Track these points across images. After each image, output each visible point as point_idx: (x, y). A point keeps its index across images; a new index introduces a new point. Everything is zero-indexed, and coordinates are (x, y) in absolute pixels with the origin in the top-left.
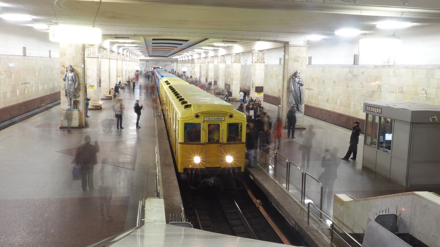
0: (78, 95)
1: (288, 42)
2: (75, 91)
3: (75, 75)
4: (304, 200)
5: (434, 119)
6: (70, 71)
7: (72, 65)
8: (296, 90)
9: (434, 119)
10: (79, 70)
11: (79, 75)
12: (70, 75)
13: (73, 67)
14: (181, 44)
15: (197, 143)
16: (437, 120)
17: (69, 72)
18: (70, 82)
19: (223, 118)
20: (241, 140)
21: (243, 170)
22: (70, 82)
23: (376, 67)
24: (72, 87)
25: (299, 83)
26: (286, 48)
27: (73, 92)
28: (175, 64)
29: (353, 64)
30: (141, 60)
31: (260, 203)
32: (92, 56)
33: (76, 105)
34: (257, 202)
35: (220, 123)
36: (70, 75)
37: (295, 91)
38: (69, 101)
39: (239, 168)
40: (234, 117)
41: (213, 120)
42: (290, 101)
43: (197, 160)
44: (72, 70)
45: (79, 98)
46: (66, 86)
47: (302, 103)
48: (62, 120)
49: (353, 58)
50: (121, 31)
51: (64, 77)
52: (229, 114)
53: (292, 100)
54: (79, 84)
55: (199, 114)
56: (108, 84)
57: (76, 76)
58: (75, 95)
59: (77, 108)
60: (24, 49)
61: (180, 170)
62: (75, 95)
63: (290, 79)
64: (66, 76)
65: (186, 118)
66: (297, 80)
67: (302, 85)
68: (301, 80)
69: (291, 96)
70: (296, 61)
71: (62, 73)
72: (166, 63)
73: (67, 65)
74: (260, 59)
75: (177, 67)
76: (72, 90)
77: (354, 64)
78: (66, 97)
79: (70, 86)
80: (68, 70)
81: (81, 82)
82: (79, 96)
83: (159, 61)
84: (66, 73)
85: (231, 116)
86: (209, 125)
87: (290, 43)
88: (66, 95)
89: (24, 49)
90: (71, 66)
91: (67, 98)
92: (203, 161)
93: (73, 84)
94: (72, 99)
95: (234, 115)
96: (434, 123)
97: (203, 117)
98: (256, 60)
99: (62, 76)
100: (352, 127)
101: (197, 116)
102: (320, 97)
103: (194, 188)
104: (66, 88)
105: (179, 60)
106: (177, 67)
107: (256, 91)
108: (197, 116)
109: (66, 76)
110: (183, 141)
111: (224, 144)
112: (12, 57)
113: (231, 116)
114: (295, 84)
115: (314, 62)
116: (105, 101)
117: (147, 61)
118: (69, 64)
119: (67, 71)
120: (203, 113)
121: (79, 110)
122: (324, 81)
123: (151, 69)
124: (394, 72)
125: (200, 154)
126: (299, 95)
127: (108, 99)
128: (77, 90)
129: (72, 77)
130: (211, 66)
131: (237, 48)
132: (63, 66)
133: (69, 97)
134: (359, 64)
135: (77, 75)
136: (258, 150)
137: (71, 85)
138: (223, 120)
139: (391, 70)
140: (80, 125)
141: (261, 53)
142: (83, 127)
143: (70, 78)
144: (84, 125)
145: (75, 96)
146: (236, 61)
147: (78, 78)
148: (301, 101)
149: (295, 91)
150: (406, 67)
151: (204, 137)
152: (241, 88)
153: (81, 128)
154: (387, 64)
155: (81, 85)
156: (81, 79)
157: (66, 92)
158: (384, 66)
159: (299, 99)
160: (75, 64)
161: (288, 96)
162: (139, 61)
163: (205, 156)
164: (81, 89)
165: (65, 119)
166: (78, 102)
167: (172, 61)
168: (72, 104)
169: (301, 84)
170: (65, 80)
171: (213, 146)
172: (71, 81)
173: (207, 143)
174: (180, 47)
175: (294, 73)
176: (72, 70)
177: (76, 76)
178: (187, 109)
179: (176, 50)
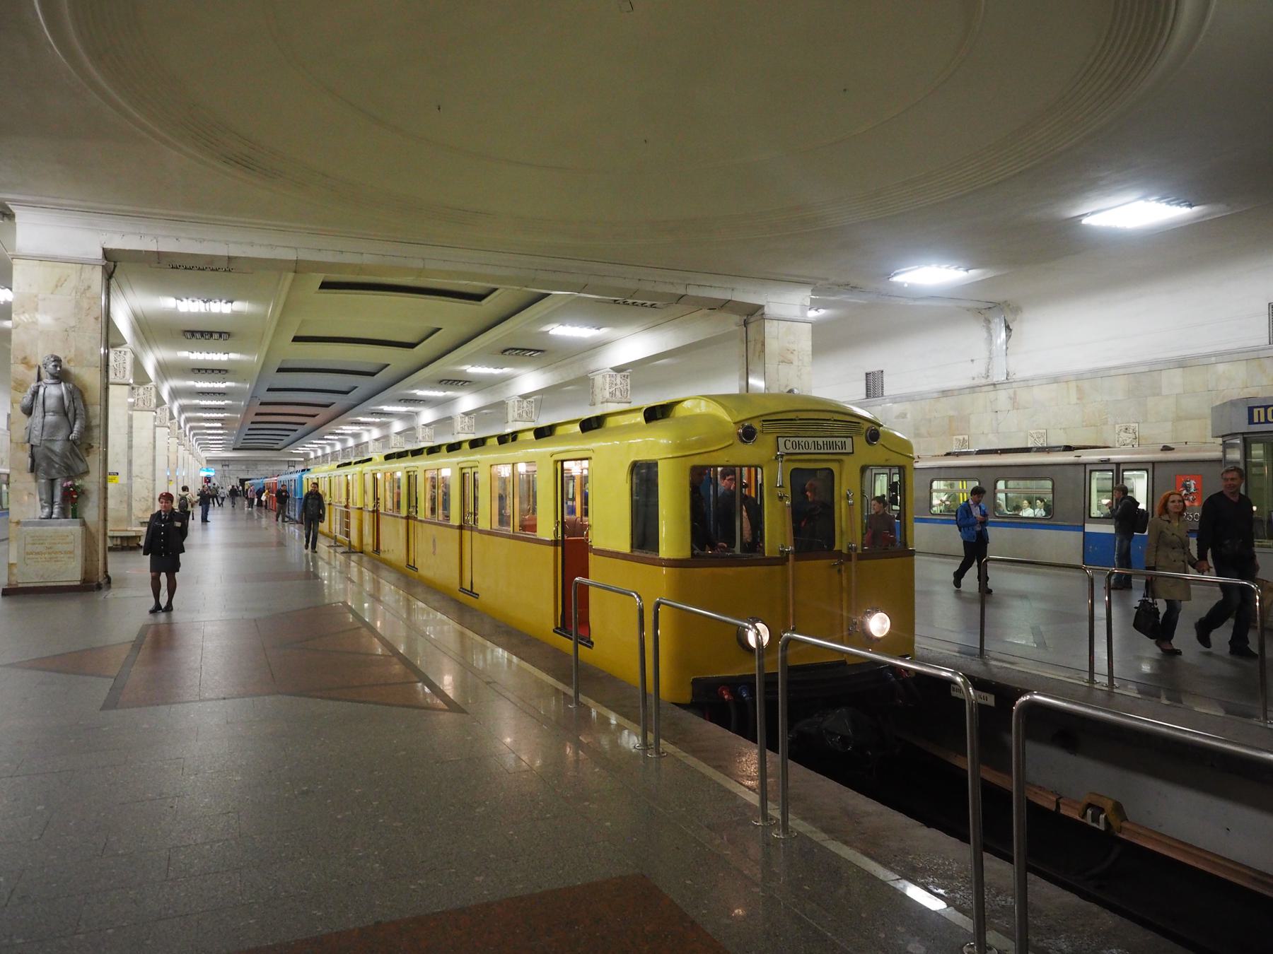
0: (81, 468)
1: (761, 307)
2: (72, 451)
3: (70, 392)
6: (53, 376)
7: (61, 356)
10: (90, 377)
12: (53, 391)
13: (65, 365)
14: (314, 416)
18: (50, 418)
19: (848, 441)
22: (50, 418)
23: (945, 393)
24: (61, 435)
26: (752, 327)
27: (63, 456)
33: (74, 502)
35: (834, 467)
36: (53, 391)
44: (61, 376)
45: (87, 478)
46: (37, 432)
48: (11, 565)
50: (252, 244)
55: (757, 425)
56: (151, 487)
57: (77, 395)
58: (68, 468)
59: (74, 517)
62: (68, 468)
64: (35, 393)
70: (786, 361)
74: (618, 393)
76: (57, 447)
77: (868, 396)
79: (52, 434)
82: (87, 472)
83: (256, 462)
84: (34, 385)
86: (796, 473)
87: (766, 310)
88: (33, 469)
90: (57, 360)
91: (36, 480)
94: (59, 482)
97: (770, 439)
98: (607, 395)
99: (19, 396)
104: (35, 441)
105: (312, 455)
108: (748, 434)
109: (35, 393)
110: (685, 553)
118: (48, 353)
119: (39, 379)
121: (84, 524)
124: (1013, 399)
129: (61, 398)
133: (47, 473)
135: (78, 393)
137: (56, 427)
138: (849, 450)
139: (1002, 396)
140: (84, 581)
142: (99, 587)
143: (51, 403)
144: (101, 579)
145: (71, 472)
146: (520, 415)
147: (85, 406)
150: (1055, 380)
152: (874, 373)
154: (984, 381)
156: (96, 410)
157: (32, 456)
158: (973, 389)
160: (72, 355)
164: (96, 445)
166: (83, 492)
168: (58, 499)
170: (28, 411)
171: (817, 568)
172: (55, 413)
174: (293, 435)
176: (61, 376)
177: (77, 395)
179: (286, 440)
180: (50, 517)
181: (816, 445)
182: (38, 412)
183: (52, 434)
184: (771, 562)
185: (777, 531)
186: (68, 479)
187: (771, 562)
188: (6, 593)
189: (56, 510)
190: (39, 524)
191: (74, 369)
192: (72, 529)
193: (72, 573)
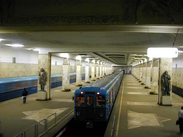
4: (45, 125)
7: (43, 68)
10: (47, 70)
25: (167, 78)
30: (113, 66)
54: (46, 78)
66: (166, 76)
71: (39, 72)
73: (41, 68)
82: (46, 84)
93: (43, 78)
100: (22, 95)
112: (32, 65)
115: (17, 61)
129: (43, 74)
130: (79, 68)
131: (79, 58)
132: (39, 68)
136: (95, 107)
143: (41, 75)
160: (45, 68)
165: (78, 96)
172: (42, 76)
175: (164, 72)
178: (146, 89)
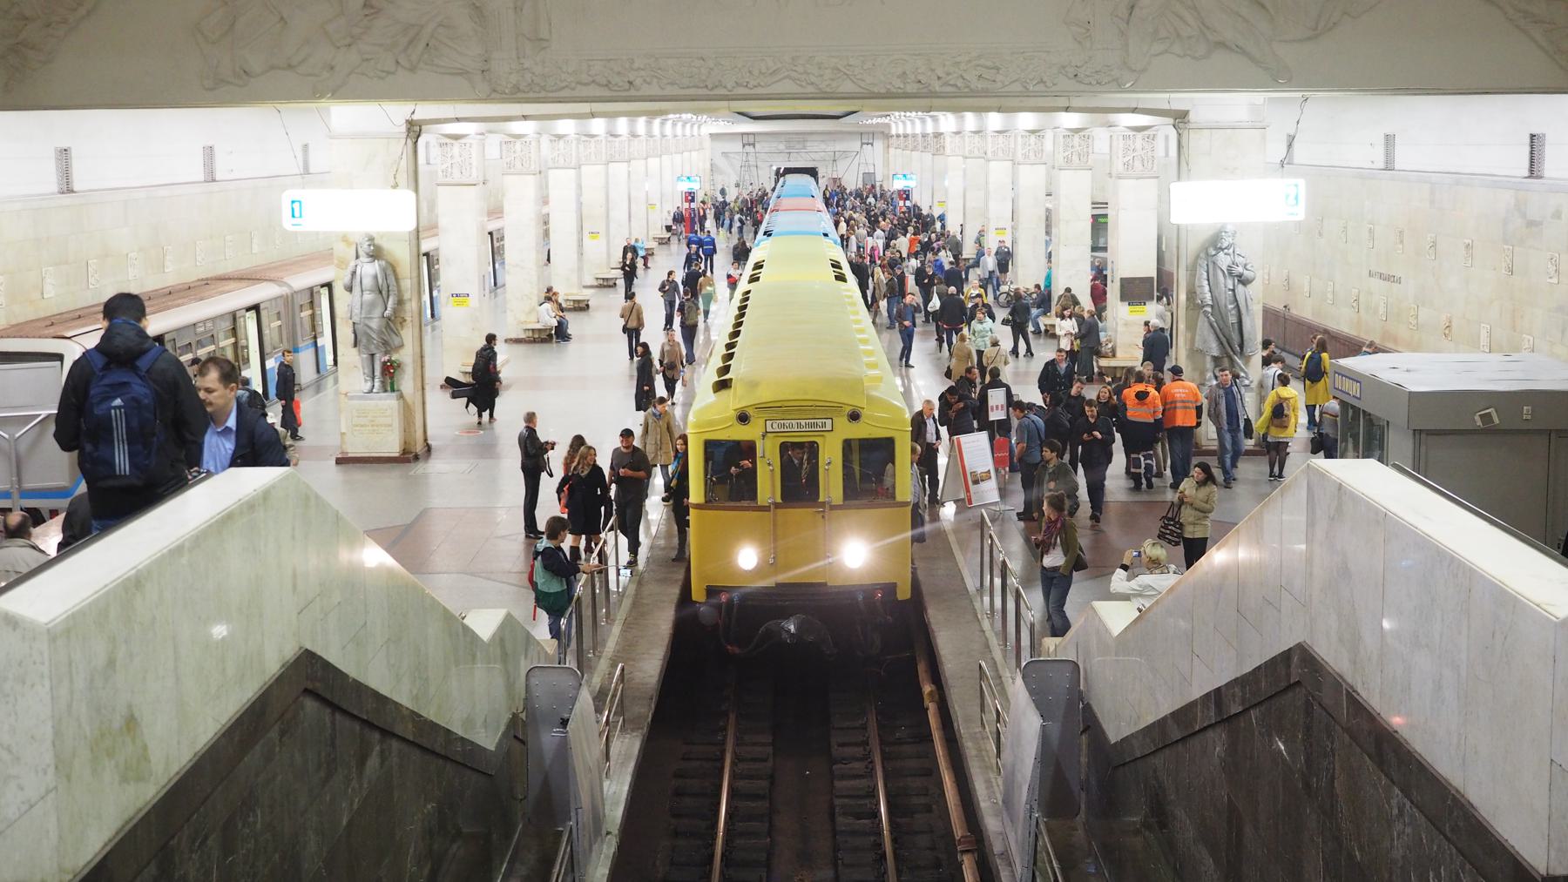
0: (397, 341)
3: (384, 270)
5: (1486, 418)
6: (369, 256)
8: (1222, 303)
9: (1486, 418)
11: (398, 270)
12: (369, 269)
15: (745, 503)
16: (1497, 421)
17: (364, 258)
18: (368, 297)
19: (829, 422)
20: (890, 494)
21: (904, 593)
22: (368, 297)
24: (377, 313)
27: (380, 332)
28: (879, 145)
29: (1527, 173)
31: (931, 693)
32: (457, 177)
33: (392, 376)
34: (927, 688)
36: (369, 269)
37: (1215, 305)
38: (367, 363)
39: (890, 589)
40: (863, 419)
41: (797, 430)
42: (1198, 345)
43: (747, 557)
44: (376, 254)
45: (402, 352)
46: (357, 311)
47: (1247, 350)
49: (1528, 149)
51: (347, 279)
52: (848, 409)
53: (1205, 342)
54: (400, 302)
55: (750, 412)
58: (385, 343)
60: (209, 152)
61: (698, 594)
62: (385, 343)
63: (1198, 257)
64: (354, 273)
65: (711, 423)
66: (1223, 260)
67: (1244, 282)
68: (1239, 260)
69: (1202, 324)
72: (839, 147)
74: (1138, 164)
75: (886, 163)
76: (374, 324)
78: (355, 351)
79: (370, 312)
80: (361, 253)
81: (407, 296)
82: (402, 346)
83: (804, 136)
84: (352, 264)
85: (855, 416)
86: (784, 447)
87: (1192, 116)
89: (209, 152)
90: (371, 239)
92: (769, 565)
93: (380, 301)
95: (865, 413)
96: (1489, 431)
101: (743, 418)
102: (1424, 314)
103: (737, 651)
104: (356, 319)
105: (894, 132)
106: (886, 163)
107: (1123, 299)
108: (743, 418)
109: (354, 273)
111: (833, 508)
113: (855, 416)
114: (1215, 275)
116: (521, 348)
117: (749, 140)
120: (761, 408)
121: (401, 397)
122: (1434, 245)
123: (764, 179)
125: (761, 541)
126: (1233, 319)
127: (534, 341)
128: (392, 323)
133: (367, 348)
134: (1547, 173)
135: (391, 270)
137: (372, 305)
140: (405, 452)
141: (1139, 135)
142: (416, 458)
143: (368, 282)
144: (419, 448)
145: (387, 347)
146: (1068, 160)
147: (397, 279)
148: (1241, 346)
149: (1215, 305)
151: (768, 484)
153: (408, 461)
155: (408, 307)
159: (1235, 337)
161: (1192, 327)
162: (707, 143)
163: (772, 541)
167: (868, 136)
169: (1240, 276)
171: (799, 514)
173: (777, 506)
176: (376, 254)
177: (389, 272)
180: (371, 391)
181: (799, 425)
182: (357, 289)
183: (370, 312)
184: (765, 509)
185: (768, 484)
186: (386, 353)
187: (765, 509)
188: (339, 461)
189: (377, 384)
190: (360, 398)
191: (386, 245)
192: (389, 402)
193: (391, 446)
